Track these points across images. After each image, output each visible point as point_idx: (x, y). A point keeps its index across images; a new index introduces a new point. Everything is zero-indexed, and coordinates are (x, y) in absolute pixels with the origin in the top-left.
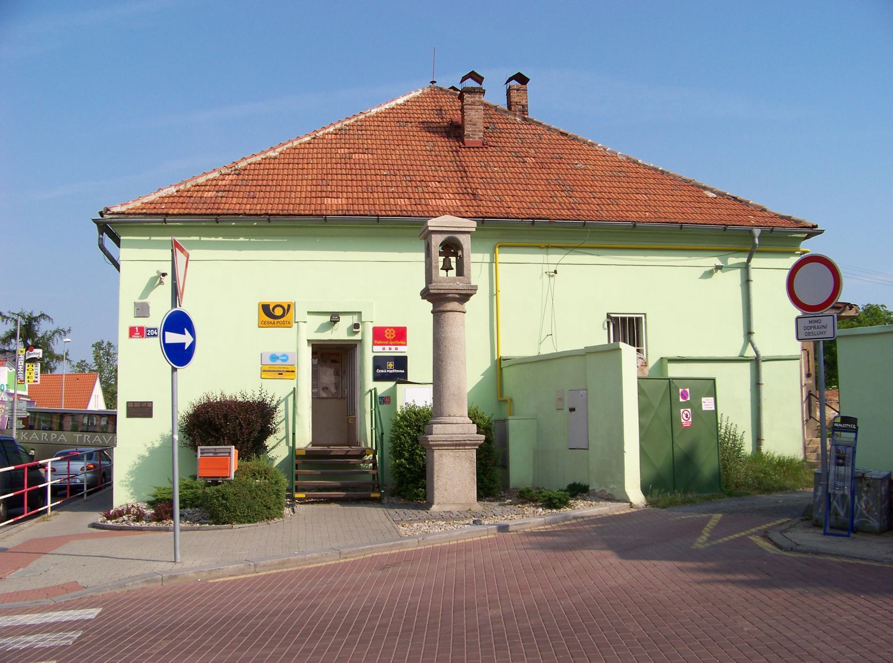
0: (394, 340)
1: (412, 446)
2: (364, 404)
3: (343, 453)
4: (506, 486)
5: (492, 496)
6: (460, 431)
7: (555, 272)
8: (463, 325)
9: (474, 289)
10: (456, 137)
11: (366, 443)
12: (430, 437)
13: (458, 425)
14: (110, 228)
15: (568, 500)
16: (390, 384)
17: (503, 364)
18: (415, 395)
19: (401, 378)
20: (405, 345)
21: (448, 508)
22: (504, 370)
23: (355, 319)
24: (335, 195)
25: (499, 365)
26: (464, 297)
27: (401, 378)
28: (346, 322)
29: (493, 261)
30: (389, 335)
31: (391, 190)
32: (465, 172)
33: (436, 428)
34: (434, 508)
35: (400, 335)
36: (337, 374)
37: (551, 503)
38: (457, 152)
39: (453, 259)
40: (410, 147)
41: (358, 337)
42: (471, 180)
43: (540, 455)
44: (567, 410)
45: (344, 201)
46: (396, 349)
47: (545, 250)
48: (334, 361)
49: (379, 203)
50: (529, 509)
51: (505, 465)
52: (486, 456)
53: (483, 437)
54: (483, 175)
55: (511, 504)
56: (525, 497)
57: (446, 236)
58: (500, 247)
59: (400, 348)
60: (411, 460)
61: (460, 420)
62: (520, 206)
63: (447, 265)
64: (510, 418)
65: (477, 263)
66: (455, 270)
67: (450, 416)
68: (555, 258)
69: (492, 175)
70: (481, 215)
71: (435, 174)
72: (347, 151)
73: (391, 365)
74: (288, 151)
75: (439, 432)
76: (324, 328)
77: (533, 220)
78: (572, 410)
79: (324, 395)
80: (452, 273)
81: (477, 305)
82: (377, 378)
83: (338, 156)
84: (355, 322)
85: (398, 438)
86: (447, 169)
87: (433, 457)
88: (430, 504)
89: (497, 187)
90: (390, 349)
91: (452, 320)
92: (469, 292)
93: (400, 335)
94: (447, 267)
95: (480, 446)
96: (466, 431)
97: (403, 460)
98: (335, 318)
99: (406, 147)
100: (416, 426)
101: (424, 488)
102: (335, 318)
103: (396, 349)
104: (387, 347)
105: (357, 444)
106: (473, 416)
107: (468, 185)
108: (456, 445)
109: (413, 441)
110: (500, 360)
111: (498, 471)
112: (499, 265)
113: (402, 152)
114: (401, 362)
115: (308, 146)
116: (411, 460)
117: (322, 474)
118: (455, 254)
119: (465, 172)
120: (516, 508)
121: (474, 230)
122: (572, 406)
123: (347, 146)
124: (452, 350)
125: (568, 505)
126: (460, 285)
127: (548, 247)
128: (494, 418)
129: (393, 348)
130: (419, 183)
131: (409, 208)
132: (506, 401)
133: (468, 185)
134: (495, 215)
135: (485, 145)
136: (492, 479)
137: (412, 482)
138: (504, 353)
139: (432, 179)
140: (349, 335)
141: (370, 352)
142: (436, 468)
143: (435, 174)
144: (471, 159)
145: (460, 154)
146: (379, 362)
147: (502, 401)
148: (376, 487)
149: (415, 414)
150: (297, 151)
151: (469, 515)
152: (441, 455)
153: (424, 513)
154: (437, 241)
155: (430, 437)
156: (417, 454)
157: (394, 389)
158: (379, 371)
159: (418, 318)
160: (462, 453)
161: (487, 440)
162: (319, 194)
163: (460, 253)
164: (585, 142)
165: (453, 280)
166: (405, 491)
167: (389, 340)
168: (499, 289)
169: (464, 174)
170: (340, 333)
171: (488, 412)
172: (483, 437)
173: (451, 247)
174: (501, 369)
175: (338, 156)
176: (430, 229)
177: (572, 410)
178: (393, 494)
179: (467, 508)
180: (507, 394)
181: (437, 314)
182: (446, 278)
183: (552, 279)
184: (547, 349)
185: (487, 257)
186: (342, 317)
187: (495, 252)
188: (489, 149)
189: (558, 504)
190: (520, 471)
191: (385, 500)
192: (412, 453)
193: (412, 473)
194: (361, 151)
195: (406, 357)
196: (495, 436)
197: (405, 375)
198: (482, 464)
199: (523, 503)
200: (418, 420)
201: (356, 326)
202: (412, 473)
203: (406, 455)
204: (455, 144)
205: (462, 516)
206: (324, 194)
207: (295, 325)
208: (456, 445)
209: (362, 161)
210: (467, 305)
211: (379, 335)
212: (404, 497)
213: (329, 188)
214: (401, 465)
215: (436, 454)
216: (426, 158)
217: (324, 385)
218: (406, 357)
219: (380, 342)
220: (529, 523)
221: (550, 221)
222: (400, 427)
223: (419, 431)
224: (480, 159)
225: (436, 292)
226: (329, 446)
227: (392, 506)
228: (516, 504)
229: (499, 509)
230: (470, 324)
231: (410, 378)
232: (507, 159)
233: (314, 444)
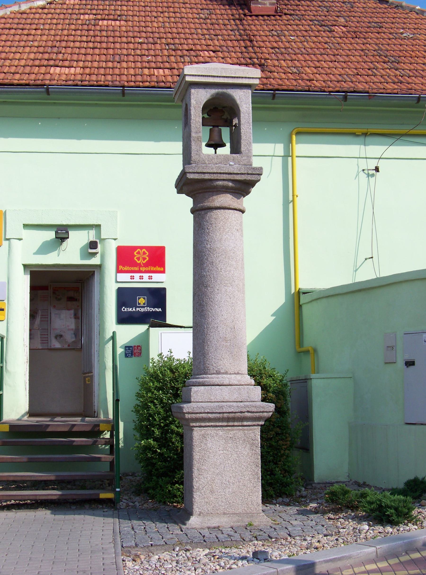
0: (146, 265)
1: (165, 418)
2: (103, 357)
3: (66, 429)
4: (308, 479)
5: (289, 495)
6: (235, 396)
7: (377, 169)
8: (240, 230)
9: (259, 172)
10: (240, 5)
11: (106, 413)
12: (186, 408)
13: (231, 386)
14: (288, 371)
15: (410, 509)
16: (141, 328)
17: (304, 299)
18: (172, 344)
19: (158, 319)
20: (164, 272)
21: (214, 522)
22: (305, 309)
23: (91, 235)
24: (67, 63)
25: (298, 301)
26: (243, 186)
27: (158, 319)
28: (77, 240)
29: (288, 155)
30: (141, 258)
31: (145, 59)
32: (251, 41)
33: (198, 393)
34: (194, 521)
35: (156, 258)
36: (76, 317)
37: (381, 515)
38: (241, 20)
39: (226, 133)
40: (178, 15)
41: (95, 261)
42: (258, 50)
43: (360, 432)
44: (401, 363)
45: (78, 70)
46: (150, 278)
47: (362, 139)
48: (71, 299)
49: (128, 72)
50: (347, 525)
51: (306, 447)
52: (277, 434)
53: (271, 407)
54: (275, 45)
55: (316, 511)
56: (341, 500)
57: (213, 91)
58: (298, 133)
59: (156, 277)
60: (164, 441)
61: (234, 379)
62: (326, 78)
63: (216, 138)
64: (313, 376)
65: (263, 153)
66: (228, 145)
67: (218, 373)
68: (375, 149)
69: (287, 45)
70: (271, 87)
71: (210, 42)
72: (91, 17)
73: (142, 301)
74: (12, 16)
75: (201, 398)
76: (46, 248)
77: (345, 95)
78: (410, 364)
79: (57, 345)
80: (225, 151)
81: (262, 200)
82: (123, 319)
83: (80, 22)
84: (92, 239)
85: (145, 406)
86: (226, 37)
87: (191, 438)
88: (187, 514)
89: (294, 57)
90: (141, 278)
91: (222, 221)
92: (249, 178)
93: (156, 258)
94: (215, 144)
95: (268, 420)
96: (244, 396)
97: (151, 441)
98: (62, 233)
99: (172, 14)
100: (173, 388)
101: (182, 483)
102: (62, 233)
103: (150, 278)
104: (137, 276)
105: (94, 414)
106: (257, 374)
107: (253, 55)
108: (228, 420)
109: (166, 411)
110: (300, 293)
111: (296, 456)
112: (296, 160)
113: (166, 19)
114: (158, 296)
115: (40, 11)
116: (164, 441)
117: (31, 461)
118: (228, 123)
119: (251, 41)
120: (323, 519)
121: (257, 82)
122: (409, 358)
123: (94, 12)
124: (222, 269)
125: (414, 521)
126: (235, 166)
127: (365, 135)
128: (289, 376)
129: (146, 276)
130: (185, 52)
131: (169, 79)
132: (307, 352)
133: (253, 55)
134: (291, 88)
135: (278, 13)
136: (285, 468)
137: (165, 475)
138: (304, 284)
139: (205, 47)
140: (82, 258)
141: (112, 281)
142: (196, 456)
143: (210, 42)
144: (259, 28)
145: (245, 22)
146: (125, 296)
147: (303, 352)
148: (108, 481)
149: (172, 371)
150: (25, 16)
151: (247, 535)
152: (204, 436)
153: (175, 529)
154: (199, 98)
155: (186, 408)
156: (173, 432)
157: (146, 335)
158: (124, 309)
159: (171, 222)
160: (237, 433)
161: (278, 410)
162: (46, 63)
163: (235, 121)
164: (412, 10)
165: (225, 158)
166: (154, 489)
167: (139, 265)
168: (296, 193)
169: (249, 43)
170: (70, 255)
171: (281, 367)
172: (271, 407)
173: (221, 113)
174: (300, 306)
175: (80, 22)
176: (188, 79)
177: (410, 364)
178: (140, 491)
179: (246, 521)
180: (309, 342)
181: (199, 212)
182: (214, 159)
183: (372, 180)
184: (366, 275)
185: (279, 149)
186: (71, 233)
187: (291, 141)
188: (284, 17)
189: (394, 517)
190: (329, 454)
191: (122, 504)
192: (165, 430)
193: (165, 460)
194: (112, 17)
195: (164, 289)
196: (291, 404)
197: (163, 315)
198: (271, 446)
199: (336, 511)
200: (175, 379)
201: (93, 245)
202: (165, 460)
203: (157, 432)
204: (237, 12)
205: (237, 537)
206: (52, 62)
207: (5, 244)
208: (228, 420)
209: (111, 28)
210: (247, 202)
211: (126, 257)
212: (152, 498)
213: (60, 56)
214: (148, 448)
215: (197, 433)
216: (198, 26)
217: (58, 332)
218: (164, 289)
219: (126, 268)
220: (349, 557)
221: (370, 95)
222: (148, 390)
223: (176, 396)
224: (271, 28)
225: (196, 176)
226: (53, 415)
227: (131, 514)
228: (324, 513)
229: (297, 522)
230: (252, 228)
231: (169, 321)
232: (308, 28)
233: (31, 413)
